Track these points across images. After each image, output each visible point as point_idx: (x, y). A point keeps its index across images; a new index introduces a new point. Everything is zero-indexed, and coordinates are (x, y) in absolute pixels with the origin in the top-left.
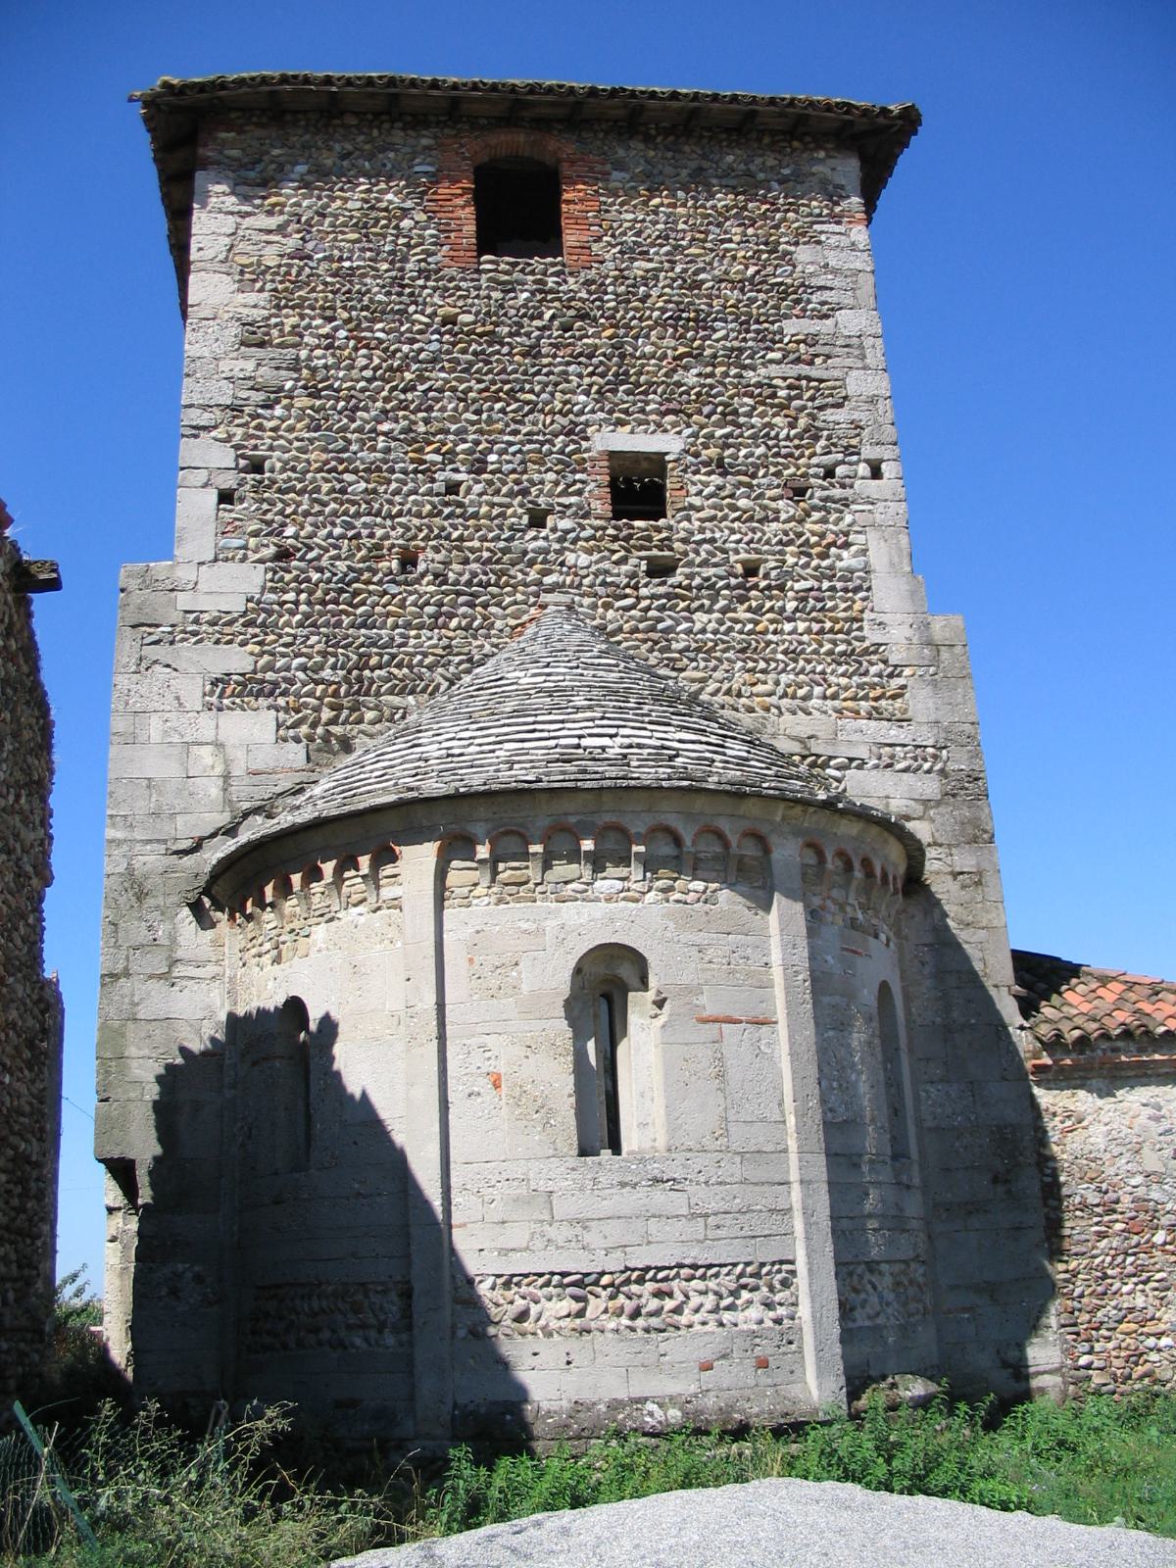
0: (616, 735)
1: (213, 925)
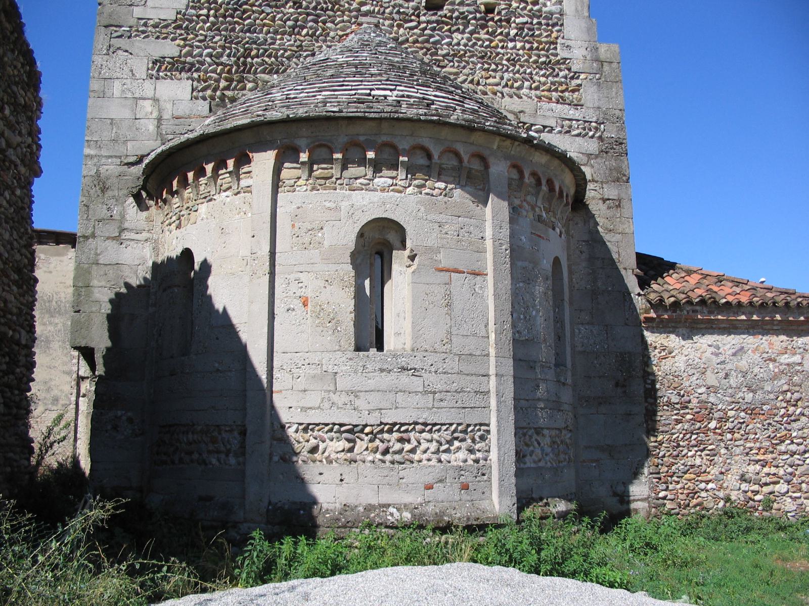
0: (394, 90)
1: (147, 208)
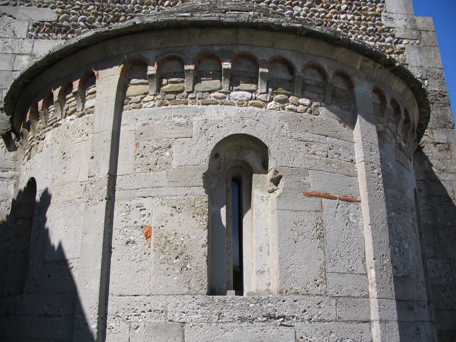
1: (15, 149)
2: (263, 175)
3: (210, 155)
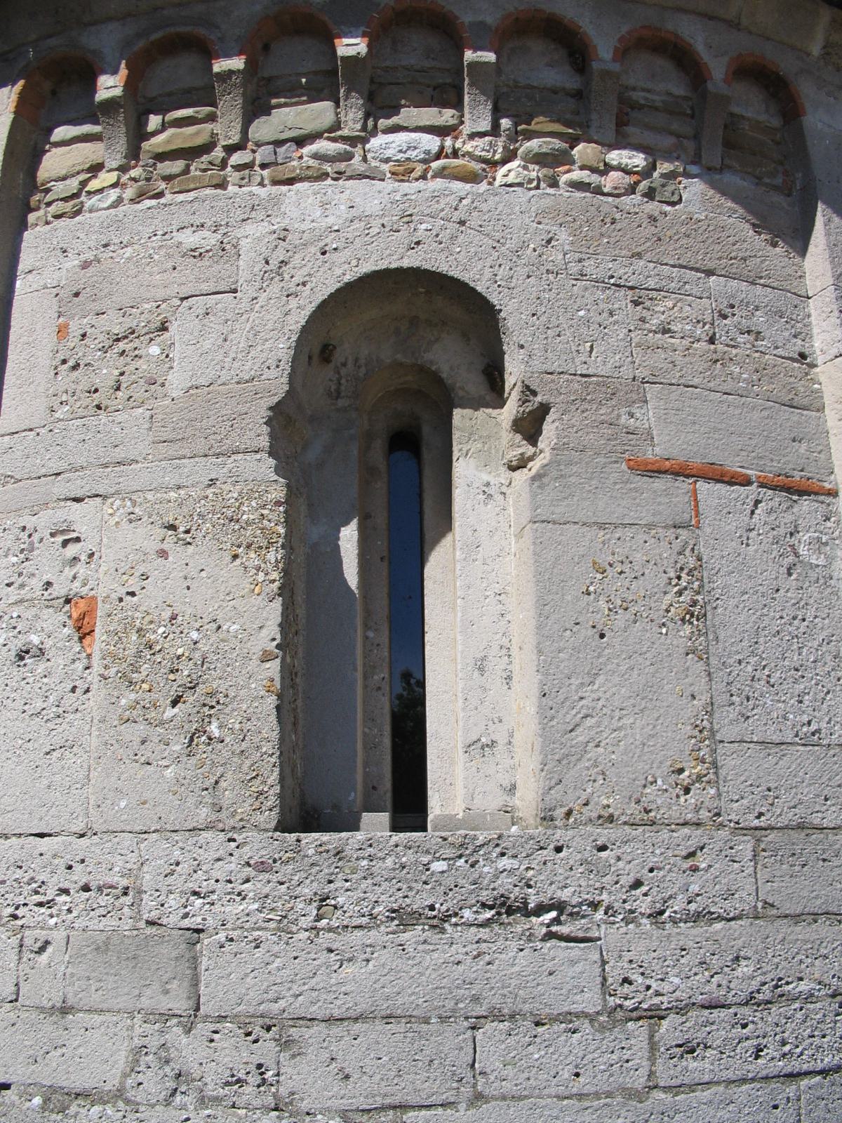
2: (490, 411)
3: (294, 344)
